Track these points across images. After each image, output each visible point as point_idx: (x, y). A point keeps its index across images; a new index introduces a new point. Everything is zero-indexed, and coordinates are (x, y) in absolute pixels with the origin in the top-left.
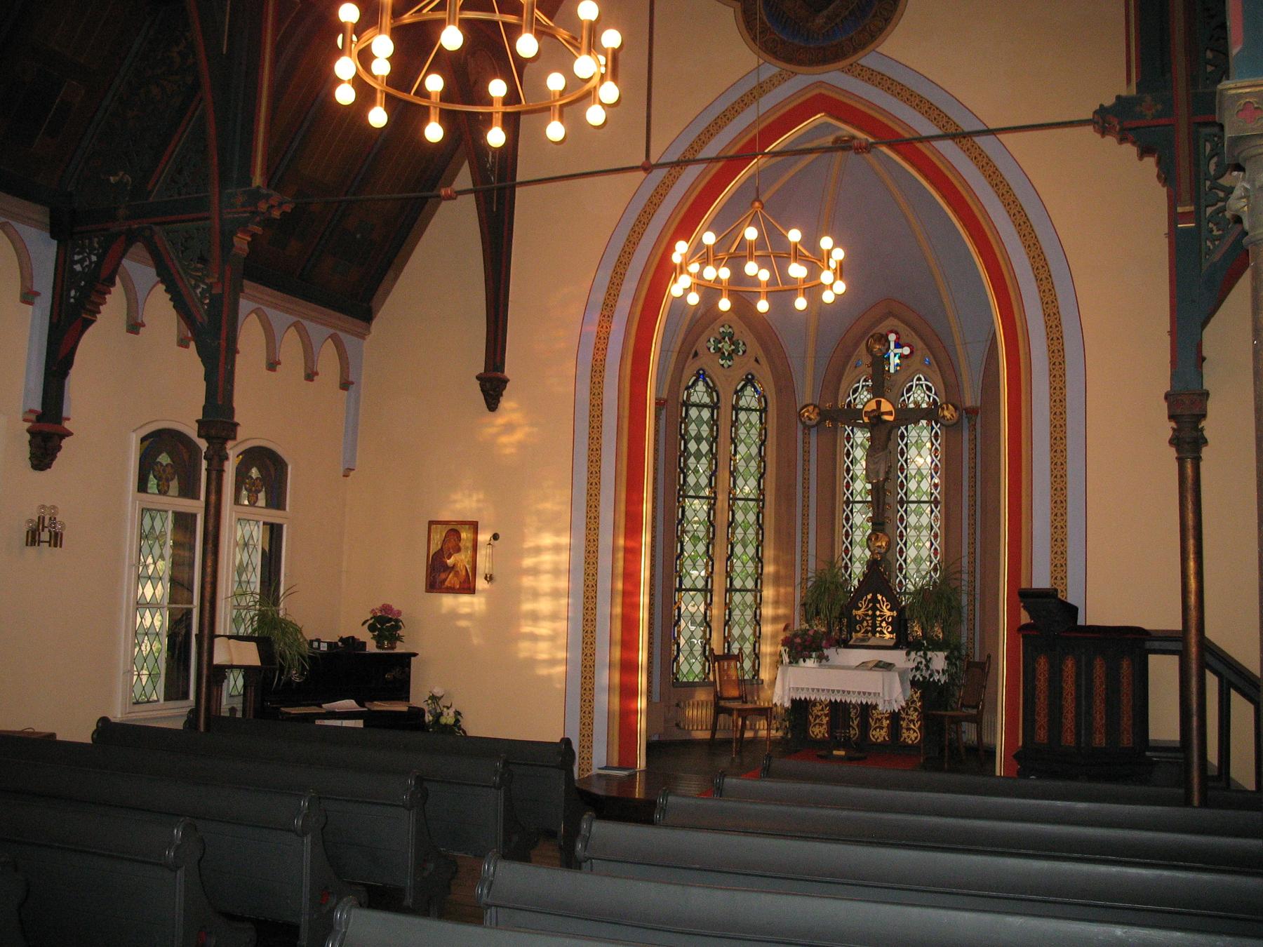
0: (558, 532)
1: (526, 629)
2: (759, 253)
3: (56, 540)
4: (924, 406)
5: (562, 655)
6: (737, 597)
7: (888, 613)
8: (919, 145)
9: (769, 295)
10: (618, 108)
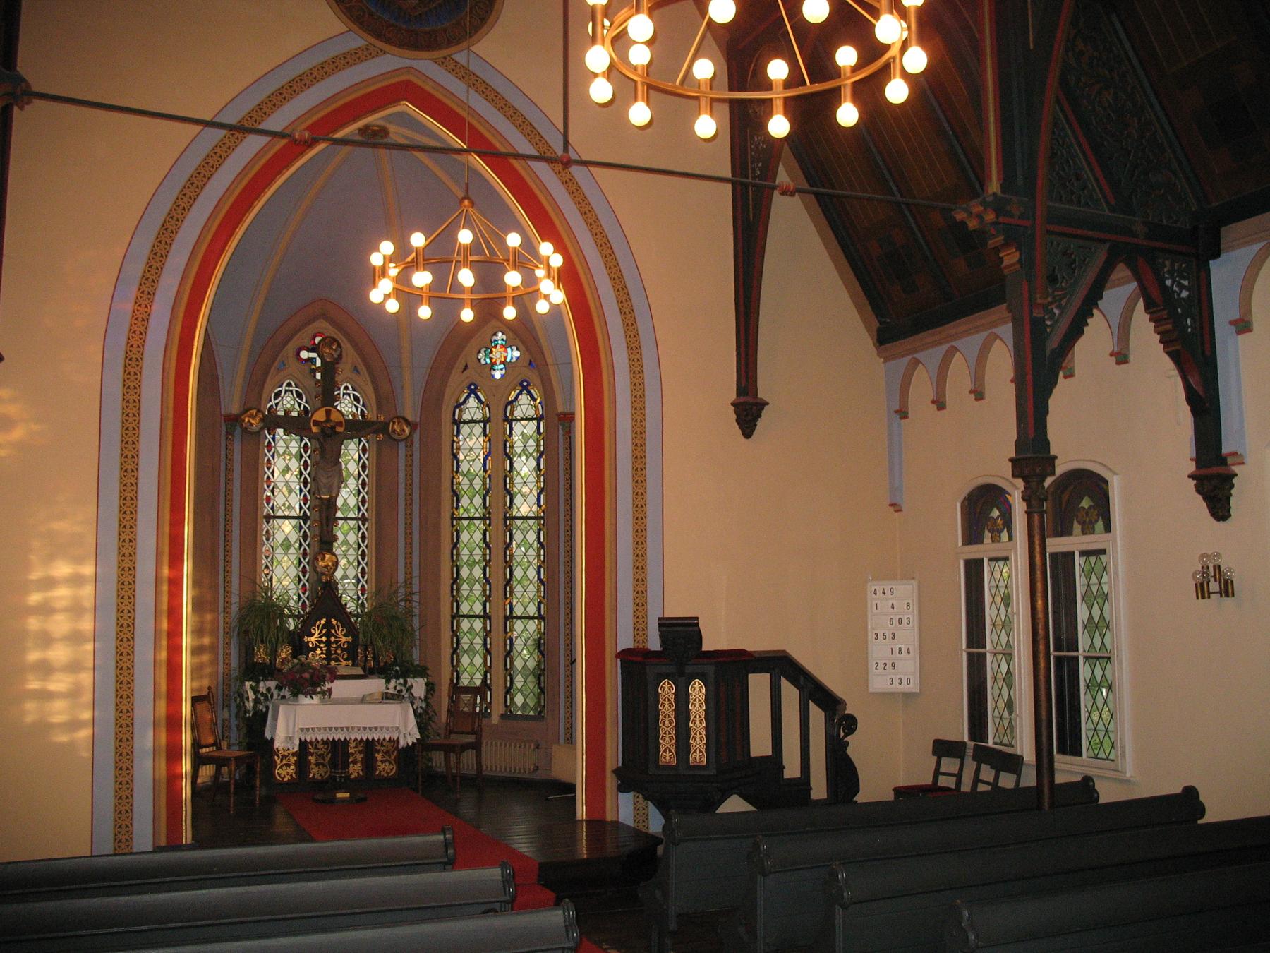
0: (79, 560)
1: (34, 685)
2: (471, 258)
3: (1227, 589)
4: (295, 414)
5: (87, 715)
6: (519, 625)
7: (344, 639)
8: (514, 162)
9: (474, 305)
10: (649, 131)
